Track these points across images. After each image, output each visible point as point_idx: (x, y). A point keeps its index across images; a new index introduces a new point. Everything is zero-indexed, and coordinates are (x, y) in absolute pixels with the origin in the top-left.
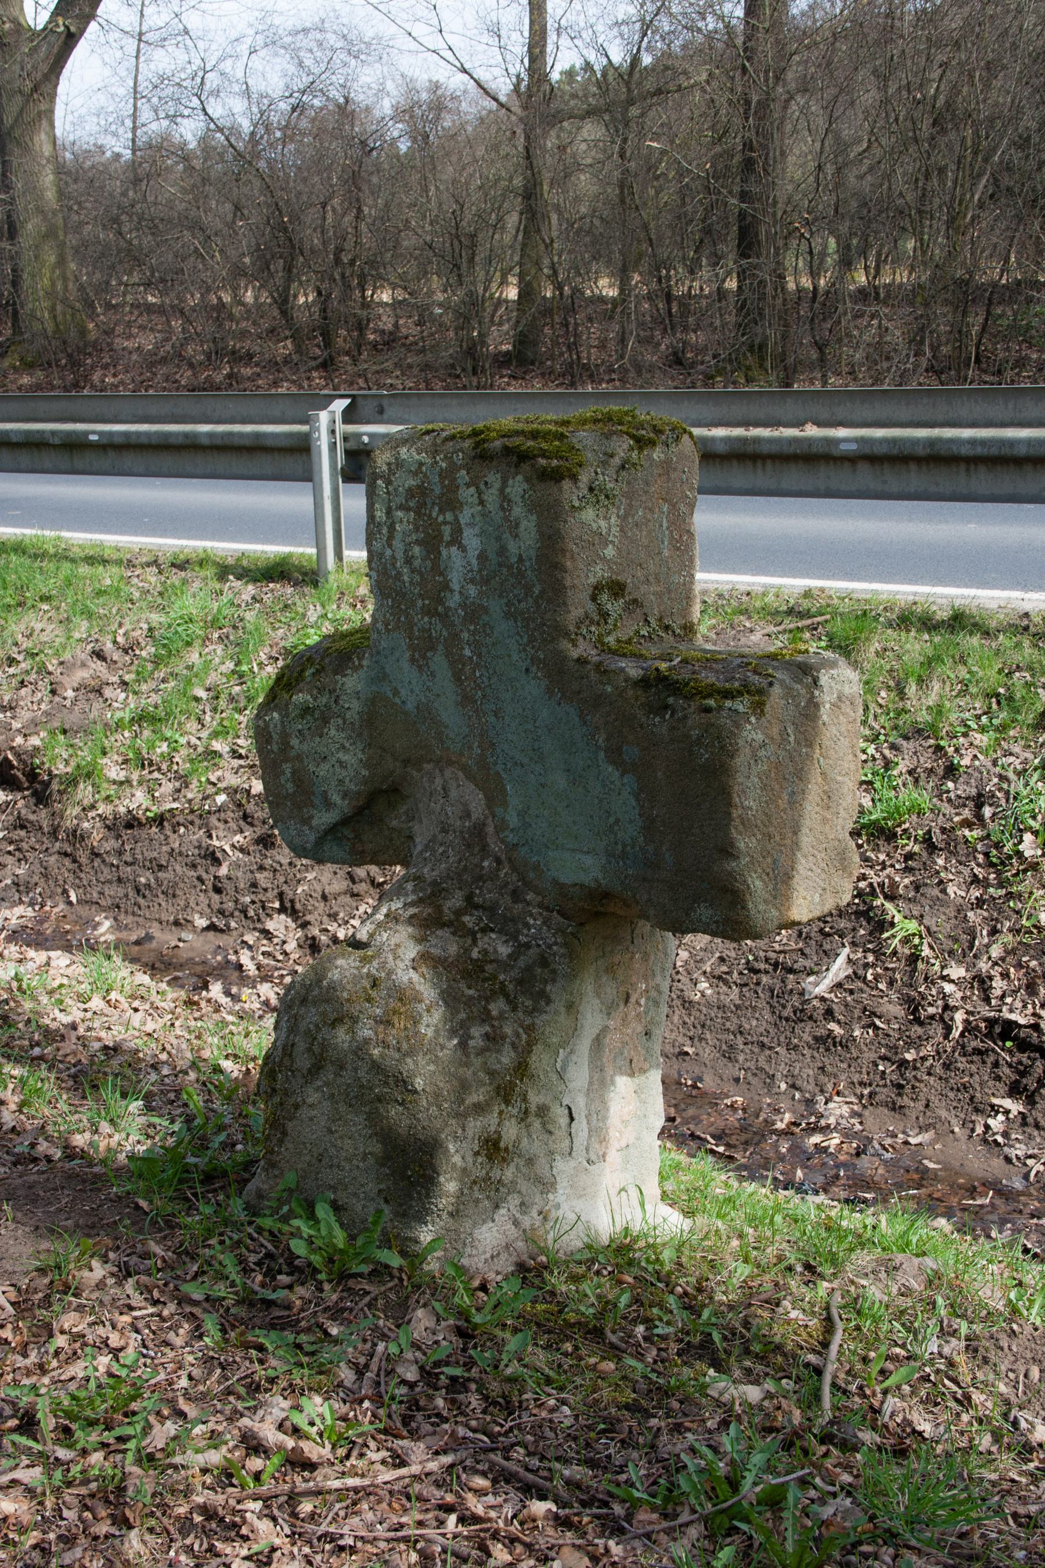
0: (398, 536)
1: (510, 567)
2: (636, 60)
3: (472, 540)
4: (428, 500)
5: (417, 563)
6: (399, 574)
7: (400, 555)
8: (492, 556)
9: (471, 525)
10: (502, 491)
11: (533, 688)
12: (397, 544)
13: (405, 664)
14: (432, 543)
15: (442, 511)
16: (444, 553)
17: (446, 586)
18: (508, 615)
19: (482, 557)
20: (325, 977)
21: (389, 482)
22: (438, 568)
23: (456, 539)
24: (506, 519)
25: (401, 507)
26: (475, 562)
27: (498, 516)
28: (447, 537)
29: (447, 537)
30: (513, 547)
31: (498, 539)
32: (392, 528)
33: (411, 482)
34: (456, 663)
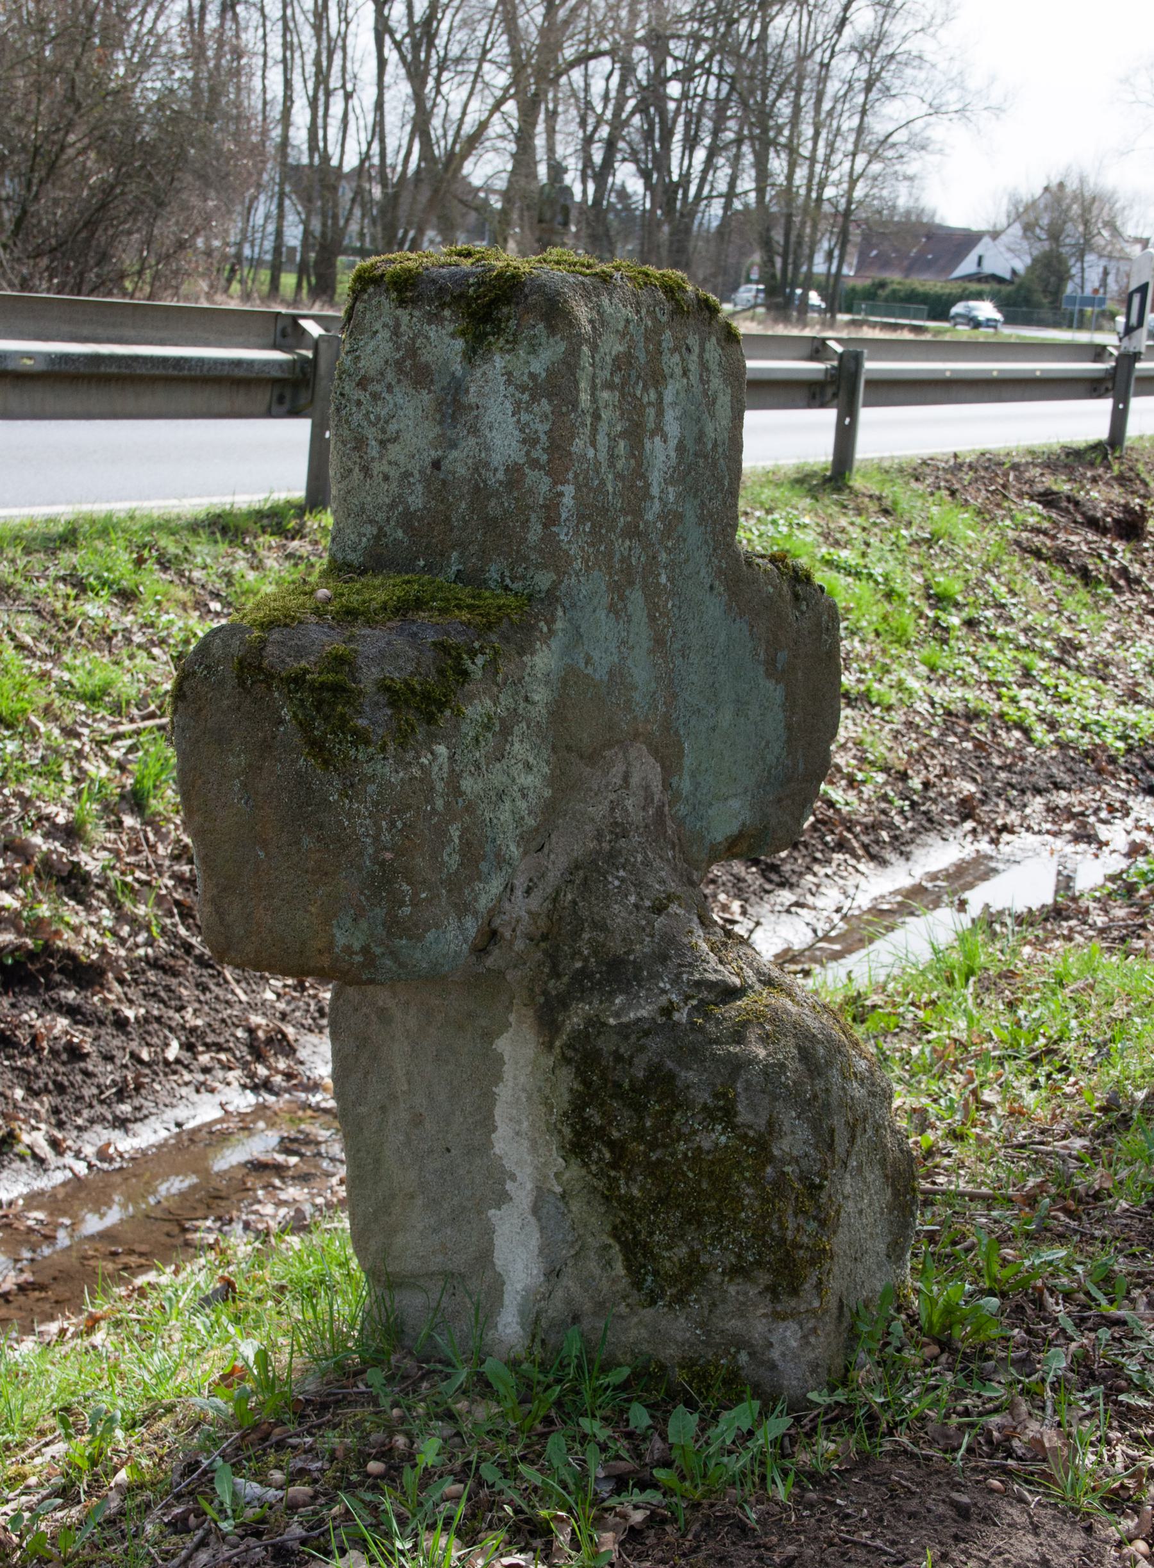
0: (603, 427)
1: (706, 457)
2: (479, 189)
3: (673, 428)
4: (634, 373)
5: (620, 465)
6: (603, 483)
7: (603, 456)
8: (690, 444)
9: (674, 404)
10: (701, 357)
11: (714, 607)
12: (602, 440)
13: (602, 614)
14: (635, 433)
15: (645, 388)
16: (648, 445)
17: (647, 495)
18: (701, 520)
19: (681, 448)
20: (131, 125)
21: (594, 348)
22: (640, 472)
23: (659, 430)
24: (705, 393)
25: (609, 386)
26: (673, 454)
27: (697, 389)
28: (651, 425)
29: (651, 425)
30: (709, 429)
31: (699, 420)
32: (597, 417)
33: (619, 348)
34: (652, 594)
